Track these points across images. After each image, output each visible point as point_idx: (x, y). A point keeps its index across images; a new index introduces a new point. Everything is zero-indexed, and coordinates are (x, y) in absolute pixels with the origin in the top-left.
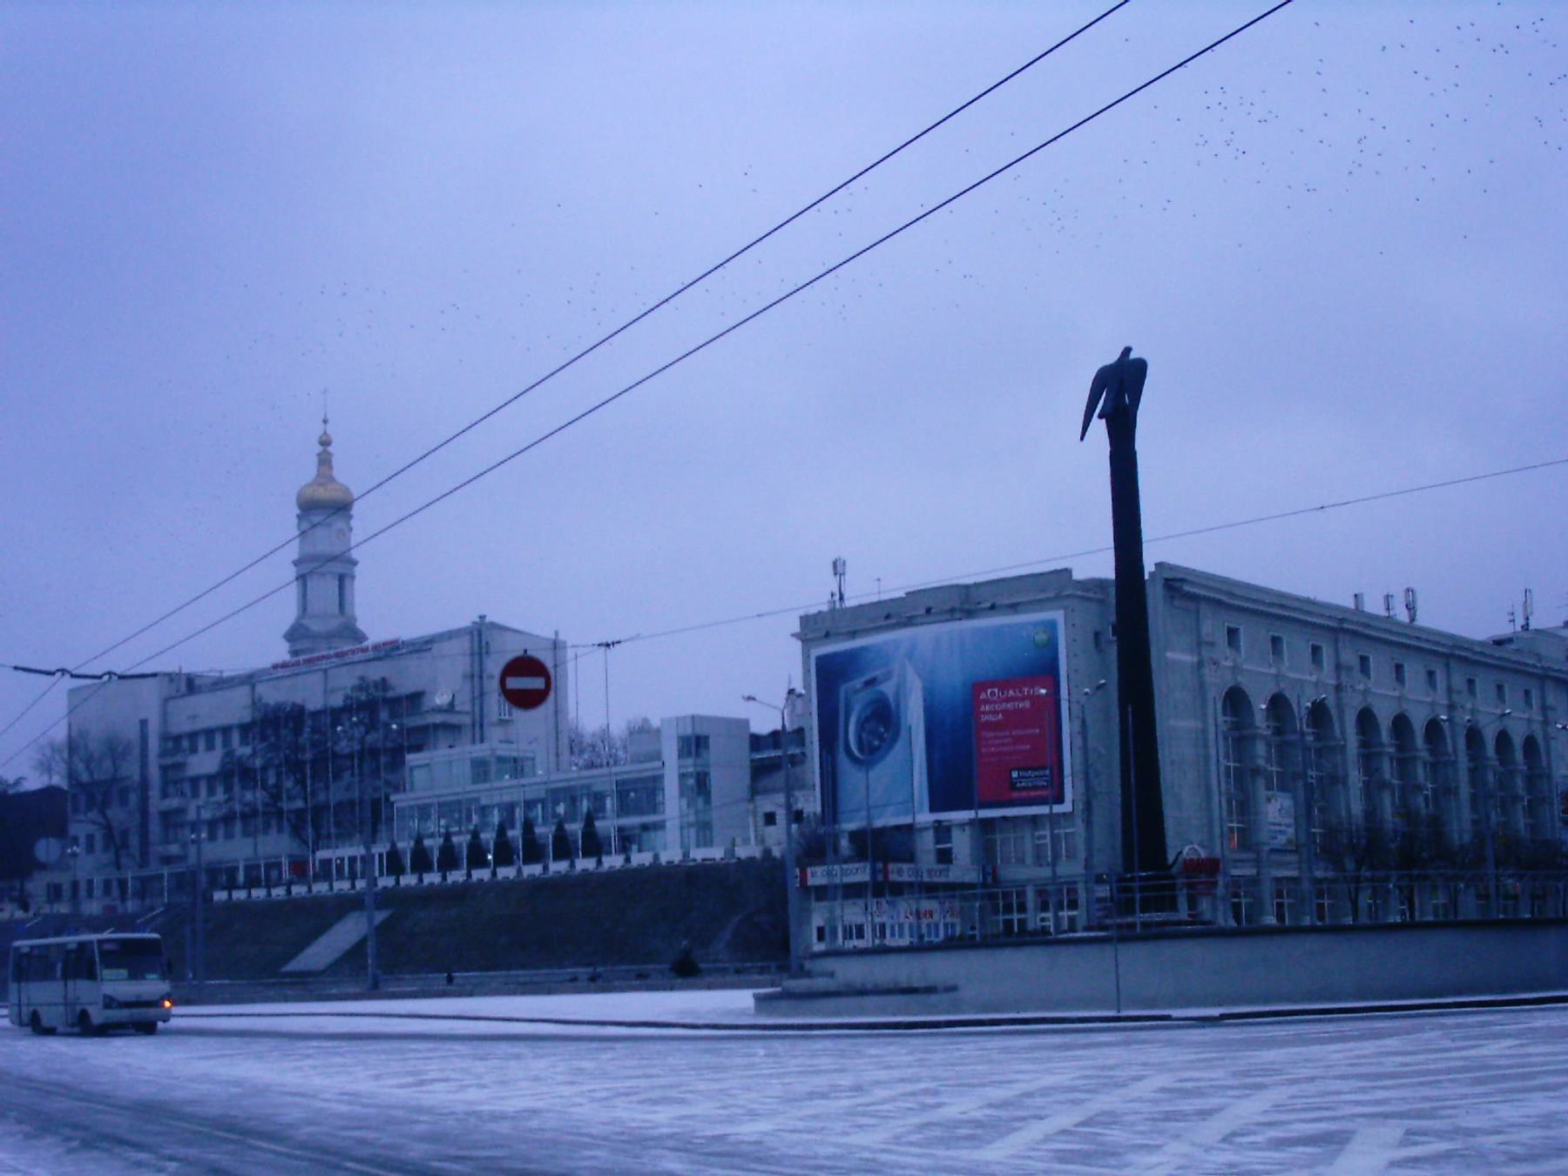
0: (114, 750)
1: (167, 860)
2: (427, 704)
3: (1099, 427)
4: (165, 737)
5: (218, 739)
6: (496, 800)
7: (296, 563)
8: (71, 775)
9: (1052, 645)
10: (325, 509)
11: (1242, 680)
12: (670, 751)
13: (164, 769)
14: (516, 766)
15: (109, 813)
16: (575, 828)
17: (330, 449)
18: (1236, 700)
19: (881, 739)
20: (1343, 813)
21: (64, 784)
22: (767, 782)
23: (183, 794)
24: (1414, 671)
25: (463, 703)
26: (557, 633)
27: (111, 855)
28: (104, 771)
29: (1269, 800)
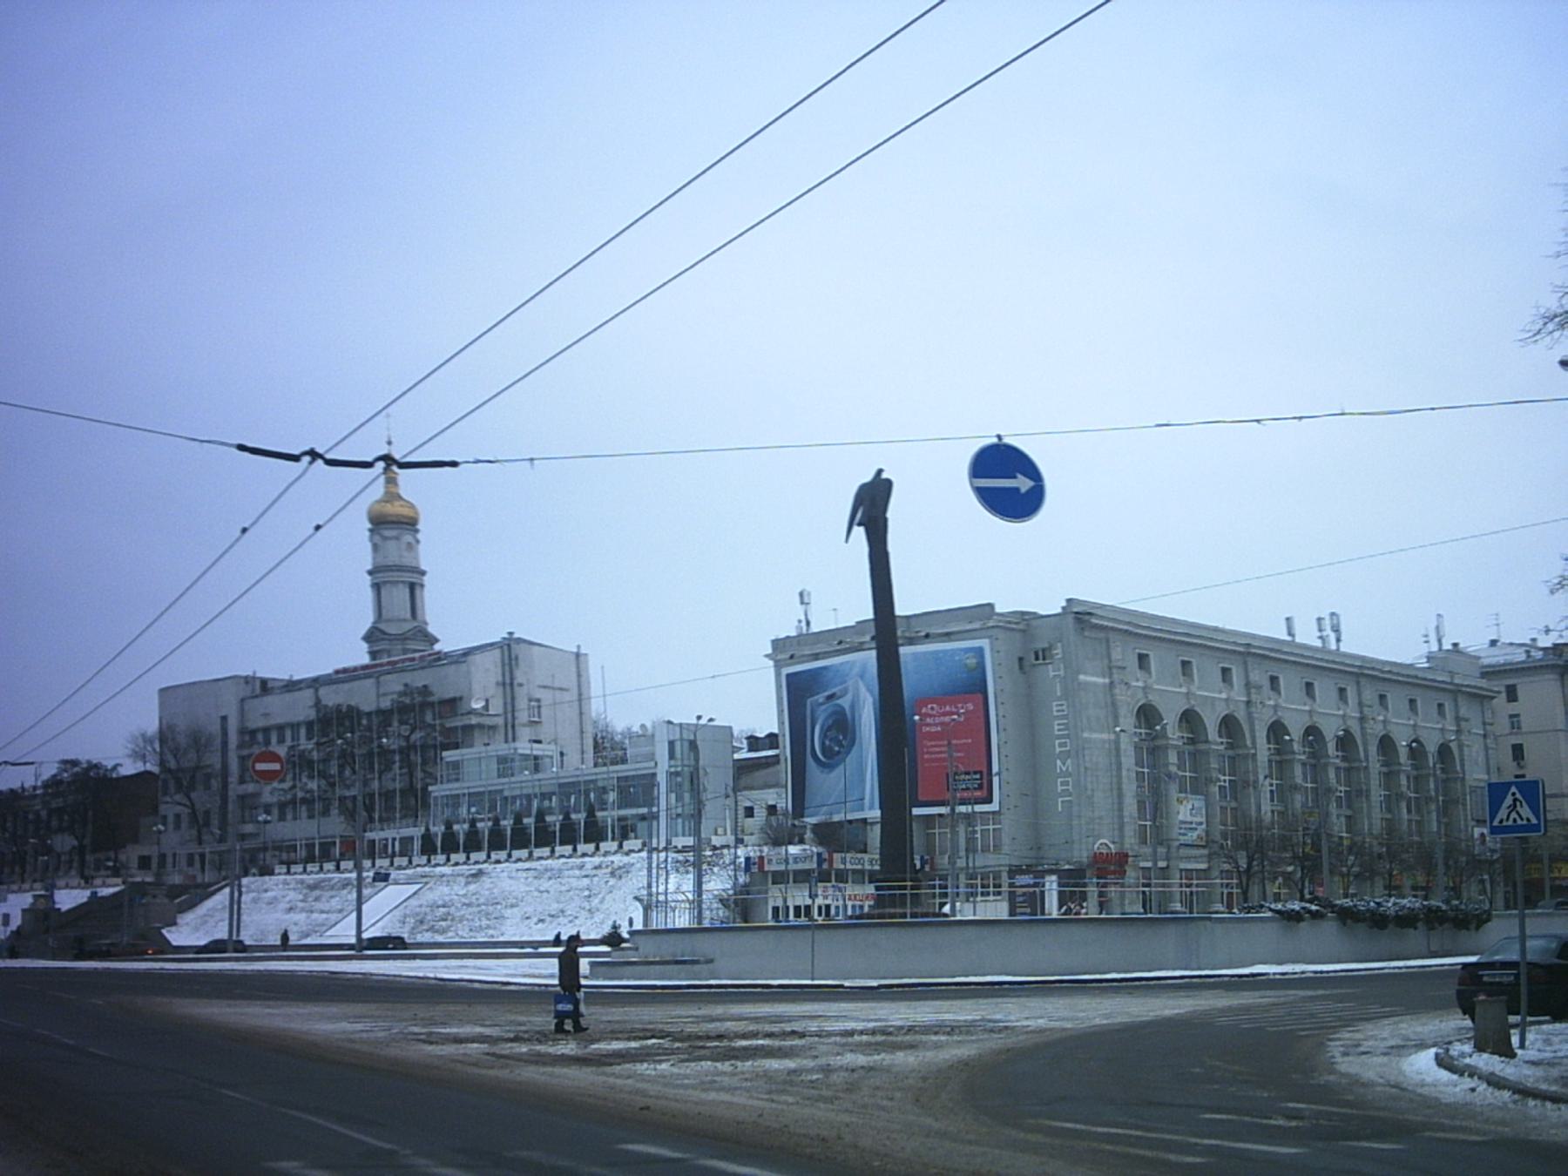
0: (198, 741)
1: (243, 837)
2: (463, 708)
3: (859, 532)
4: (243, 731)
5: (288, 733)
6: (518, 792)
7: (370, 573)
8: (162, 763)
9: (981, 666)
11: (1154, 699)
12: (662, 752)
13: (242, 759)
14: (536, 763)
15: (193, 795)
16: (579, 817)
18: (1147, 715)
19: (841, 746)
20: (1253, 814)
21: (156, 770)
22: (744, 781)
24: (1325, 688)
25: (496, 707)
26: (999, 437)
27: (194, 832)
28: (189, 760)
29: (1180, 801)
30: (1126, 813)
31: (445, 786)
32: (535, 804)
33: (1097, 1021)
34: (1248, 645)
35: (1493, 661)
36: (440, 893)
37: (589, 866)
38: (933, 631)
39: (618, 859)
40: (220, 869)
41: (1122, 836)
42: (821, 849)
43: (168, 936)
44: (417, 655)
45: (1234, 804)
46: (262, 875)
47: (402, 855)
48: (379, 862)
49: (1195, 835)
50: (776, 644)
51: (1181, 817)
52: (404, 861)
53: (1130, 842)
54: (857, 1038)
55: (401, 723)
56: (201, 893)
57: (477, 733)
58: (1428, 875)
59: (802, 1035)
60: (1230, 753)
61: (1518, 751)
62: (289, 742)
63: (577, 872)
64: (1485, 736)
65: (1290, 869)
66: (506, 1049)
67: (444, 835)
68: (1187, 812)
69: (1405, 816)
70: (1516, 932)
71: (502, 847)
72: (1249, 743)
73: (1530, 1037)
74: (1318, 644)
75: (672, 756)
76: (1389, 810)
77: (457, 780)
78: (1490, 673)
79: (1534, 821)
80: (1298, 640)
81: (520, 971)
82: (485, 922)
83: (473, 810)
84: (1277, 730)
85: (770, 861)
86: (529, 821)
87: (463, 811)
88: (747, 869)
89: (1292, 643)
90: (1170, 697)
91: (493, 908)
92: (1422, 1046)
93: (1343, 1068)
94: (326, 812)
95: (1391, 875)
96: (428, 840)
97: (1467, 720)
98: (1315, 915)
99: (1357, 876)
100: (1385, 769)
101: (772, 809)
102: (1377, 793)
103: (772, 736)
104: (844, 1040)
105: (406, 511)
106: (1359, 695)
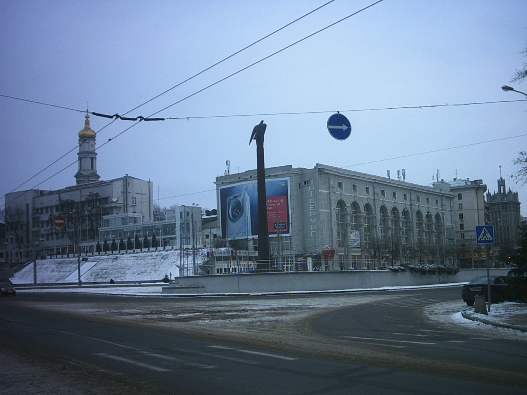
0: (18, 212)
3: (254, 141)
4: (34, 209)
5: (49, 210)
7: (78, 154)
8: (6, 220)
10: (87, 138)
11: (343, 198)
12: (178, 216)
13: (33, 219)
14: (135, 220)
15: (17, 231)
16: (150, 238)
17: (89, 119)
18: (341, 204)
19: (238, 214)
21: (4, 223)
22: (205, 226)
23: (39, 226)
24: (399, 195)
25: (121, 201)
26: (338, 112)
29: (351, 233)
30: (334, 237)
31: (104, 228)
32: (135, 234)
33: (342, 305)
34: (375, 180)
35: (454, 186)
36: (103, 265)
37: (154, 255)
38: (271, 174)
39: (164, 253)
40: (27, 257)
41: (332, 244)
42: (232, 249)
43: (11, 280)
44: (94, 182)
45: (369, 234)
46: (42, 259)
47: (90, 252)
48: (82, 255)
49: (356, 244)
50: (217, 178)
51: (352, 238)
52: (91, 254)
53: (335, 246)
54: (266, 311)
55: (89, 206)
56: (22, 266)
57: (114, 210)
58: (433, 257)
59: (247, 311)
60: (368, 216)
61: (461, 216)
62: (49, 213)
63: (150, 257)
64: (451, 211)
65: (388, 255)
66: (150, 316)
67: (104, 245)
68: (354, 236)
69: (425, 238)
70: (486, 275)
71: (124, 249)
72: (374, 213)
73: (491, 308)
74: (397, 179)
75: (181, 217)
76: (420, 236)
77: (108, 226)
78: (453, 189)
79: (491, 239)
80: (391, 178)
81: (132, 291)
82: (119, 275)
83: (113, 236)
84: (383, 209)
85: (215, 253)
86: (133, 240)
87: (110, 237)
88: (208, 256)
89: (389, 179)
90: (348, 198)
91: (122, 270)
92: (454, 312)
93: (432, 318)
94: (63, 237)
95: (421, 257)
96: (98, 246)
97: (445, 206)
98: (403, 270)
99: (410, 257)
100: (418, 222)
101: (215, 236)
102: (416, 230)
103: (214, 210)
104: (262, 312)
105: (92, 134)
106: (411, 197)
